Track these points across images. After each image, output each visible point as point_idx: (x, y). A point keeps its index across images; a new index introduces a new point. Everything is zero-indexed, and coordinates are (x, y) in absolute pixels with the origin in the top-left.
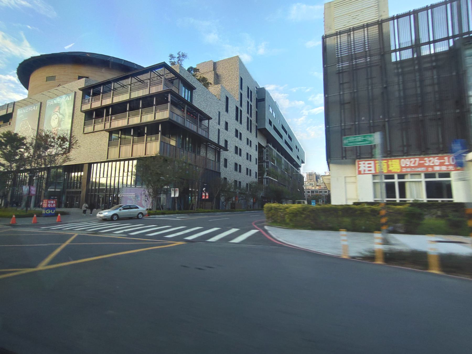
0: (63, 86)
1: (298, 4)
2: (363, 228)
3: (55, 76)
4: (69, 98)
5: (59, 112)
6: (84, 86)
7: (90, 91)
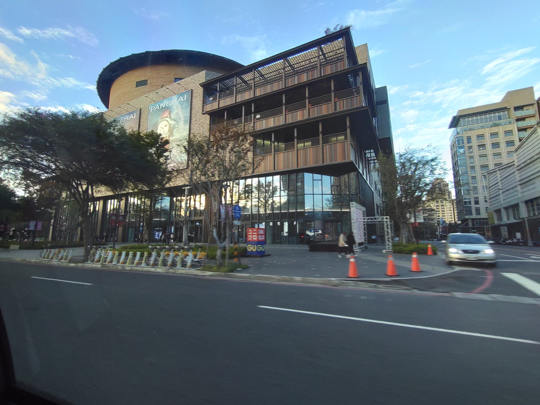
0: (167, 87)
1: (356, 11)
2: (414, 256)
3: (147, 80)
4: (184, 98)
5: (170, 117)
6: (204, 81)
7: (209, 89)
